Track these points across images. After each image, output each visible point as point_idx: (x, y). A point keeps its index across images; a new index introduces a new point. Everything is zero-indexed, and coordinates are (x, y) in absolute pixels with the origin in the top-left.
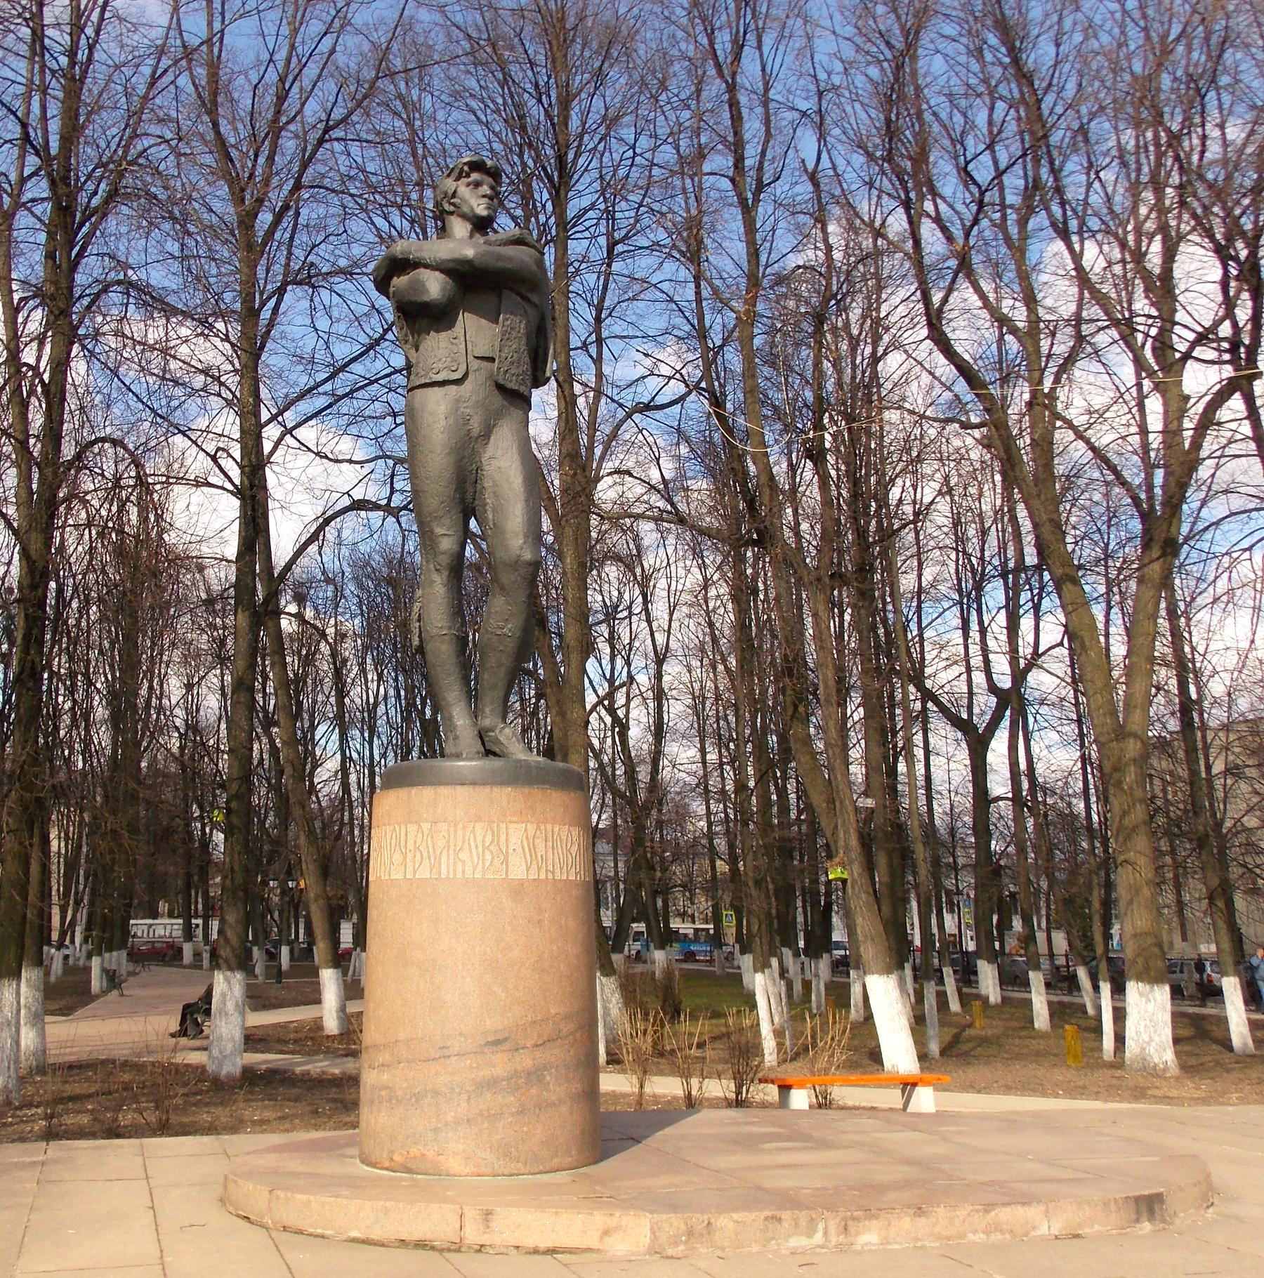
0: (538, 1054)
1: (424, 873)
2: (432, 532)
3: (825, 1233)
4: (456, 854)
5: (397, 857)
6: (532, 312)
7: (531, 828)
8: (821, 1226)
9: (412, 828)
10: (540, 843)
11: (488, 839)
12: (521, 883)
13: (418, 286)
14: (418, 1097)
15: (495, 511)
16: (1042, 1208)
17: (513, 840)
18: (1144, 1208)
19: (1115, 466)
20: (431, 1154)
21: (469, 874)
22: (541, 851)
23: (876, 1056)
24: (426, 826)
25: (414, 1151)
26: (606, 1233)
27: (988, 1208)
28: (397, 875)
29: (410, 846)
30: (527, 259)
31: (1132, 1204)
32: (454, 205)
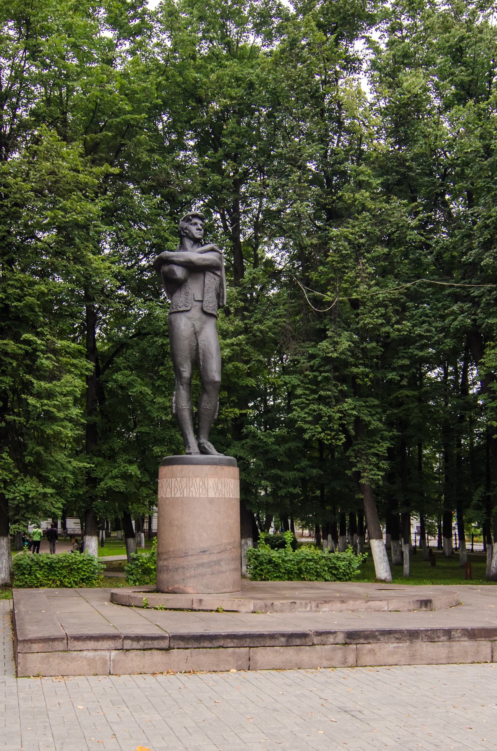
0: (218, 555)
1: (178, 495)
2: (179, 370)
3: (311, 608)
4: (190, 489)
5: (168, 490)
6: (217, 278)
7: (216, 480)
8: (309, 605)
9: (174, 480)
10: (220, 485)
11: (201, 483)
12: (213, 499)
13: (173, 272)
14: (177, 569)
15: (203, 362)
16: (386, 602)
17: (210, 484)
18: (423, 604)
19: (32, 643)
20: (182, 587)
21: (194, 496)
22: (220, 488)
23: (372, 569)
24: (179, 479)
25: (176, 586)
26: (239, 606)
27: (367, 601)
28: (168, 496)
29: (173, 486)
30: (215, 258)
31: (419, 603)
32: (186, 233)
